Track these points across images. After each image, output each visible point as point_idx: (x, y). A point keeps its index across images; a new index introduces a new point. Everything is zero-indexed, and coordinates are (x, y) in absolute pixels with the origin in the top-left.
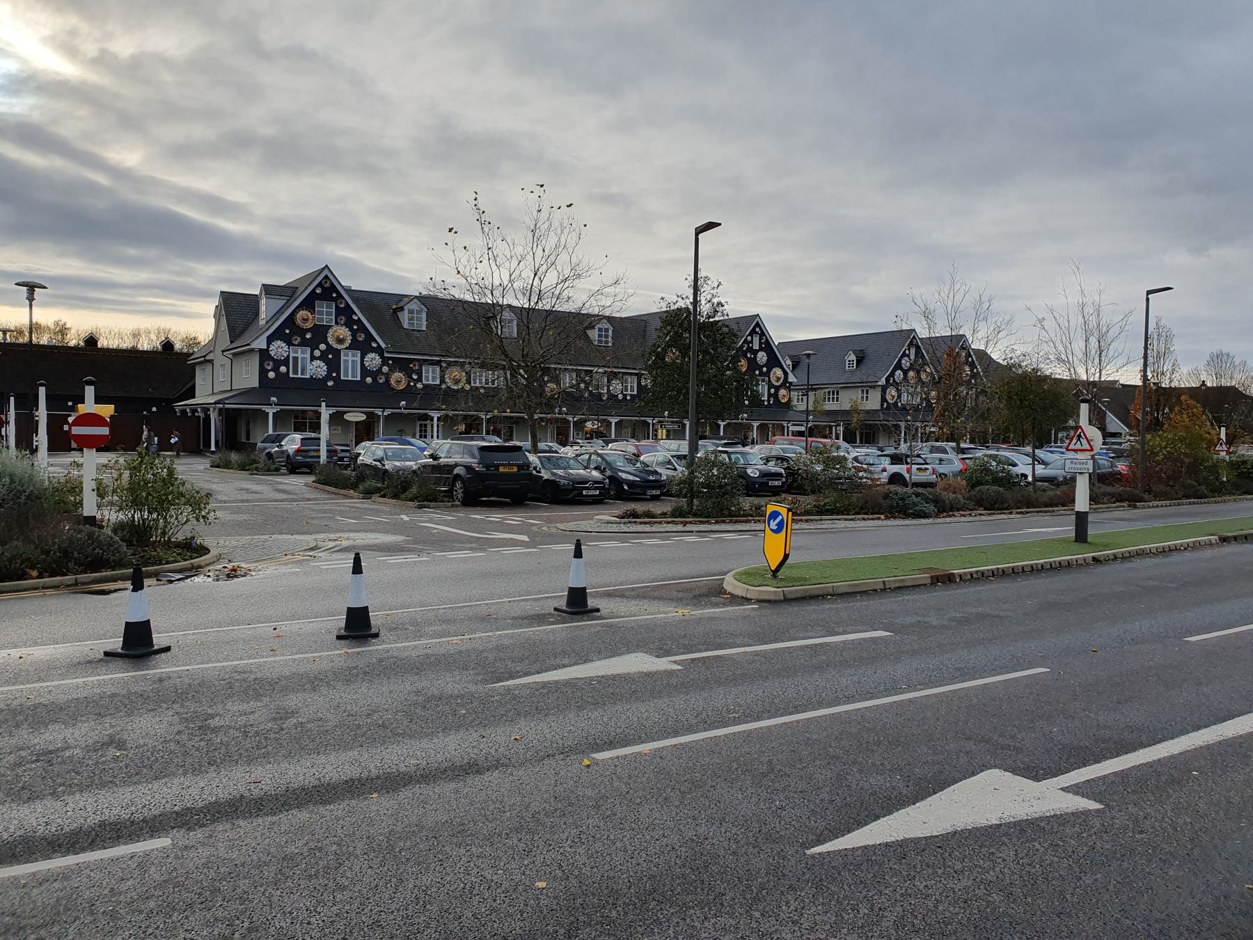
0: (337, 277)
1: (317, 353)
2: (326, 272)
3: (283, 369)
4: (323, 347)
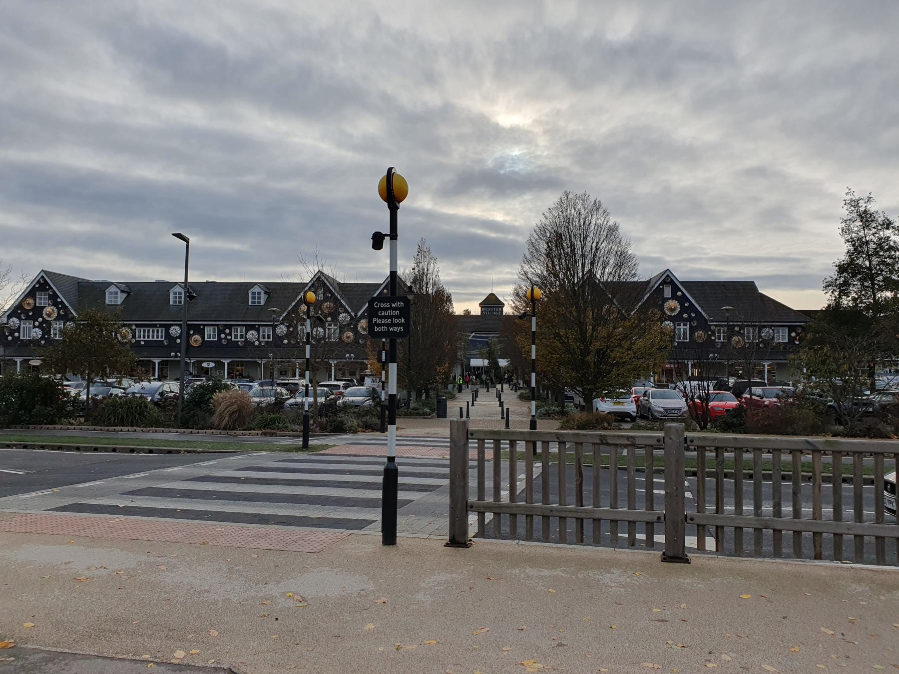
0: (37, 274)
1: (37, 324)
2: (668, 273)
3: (16, 334)
4: (40, 319)
